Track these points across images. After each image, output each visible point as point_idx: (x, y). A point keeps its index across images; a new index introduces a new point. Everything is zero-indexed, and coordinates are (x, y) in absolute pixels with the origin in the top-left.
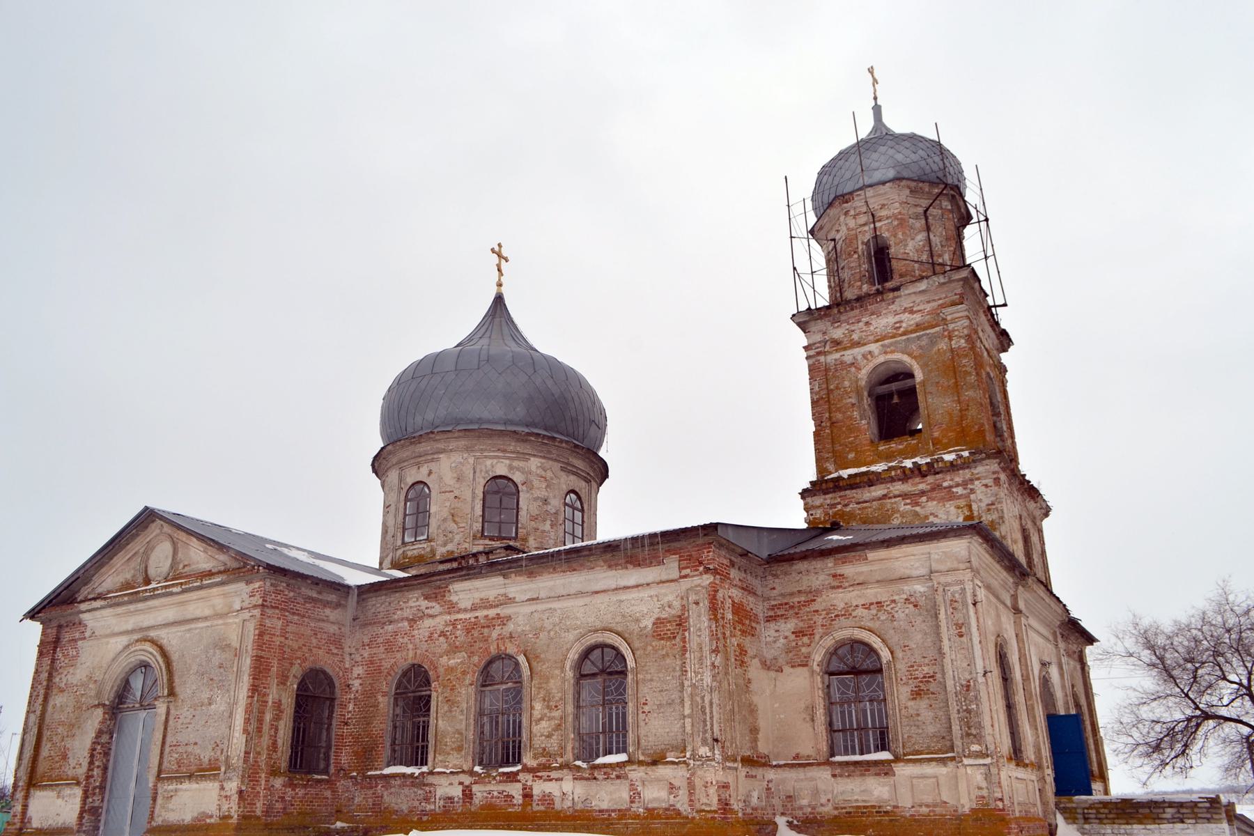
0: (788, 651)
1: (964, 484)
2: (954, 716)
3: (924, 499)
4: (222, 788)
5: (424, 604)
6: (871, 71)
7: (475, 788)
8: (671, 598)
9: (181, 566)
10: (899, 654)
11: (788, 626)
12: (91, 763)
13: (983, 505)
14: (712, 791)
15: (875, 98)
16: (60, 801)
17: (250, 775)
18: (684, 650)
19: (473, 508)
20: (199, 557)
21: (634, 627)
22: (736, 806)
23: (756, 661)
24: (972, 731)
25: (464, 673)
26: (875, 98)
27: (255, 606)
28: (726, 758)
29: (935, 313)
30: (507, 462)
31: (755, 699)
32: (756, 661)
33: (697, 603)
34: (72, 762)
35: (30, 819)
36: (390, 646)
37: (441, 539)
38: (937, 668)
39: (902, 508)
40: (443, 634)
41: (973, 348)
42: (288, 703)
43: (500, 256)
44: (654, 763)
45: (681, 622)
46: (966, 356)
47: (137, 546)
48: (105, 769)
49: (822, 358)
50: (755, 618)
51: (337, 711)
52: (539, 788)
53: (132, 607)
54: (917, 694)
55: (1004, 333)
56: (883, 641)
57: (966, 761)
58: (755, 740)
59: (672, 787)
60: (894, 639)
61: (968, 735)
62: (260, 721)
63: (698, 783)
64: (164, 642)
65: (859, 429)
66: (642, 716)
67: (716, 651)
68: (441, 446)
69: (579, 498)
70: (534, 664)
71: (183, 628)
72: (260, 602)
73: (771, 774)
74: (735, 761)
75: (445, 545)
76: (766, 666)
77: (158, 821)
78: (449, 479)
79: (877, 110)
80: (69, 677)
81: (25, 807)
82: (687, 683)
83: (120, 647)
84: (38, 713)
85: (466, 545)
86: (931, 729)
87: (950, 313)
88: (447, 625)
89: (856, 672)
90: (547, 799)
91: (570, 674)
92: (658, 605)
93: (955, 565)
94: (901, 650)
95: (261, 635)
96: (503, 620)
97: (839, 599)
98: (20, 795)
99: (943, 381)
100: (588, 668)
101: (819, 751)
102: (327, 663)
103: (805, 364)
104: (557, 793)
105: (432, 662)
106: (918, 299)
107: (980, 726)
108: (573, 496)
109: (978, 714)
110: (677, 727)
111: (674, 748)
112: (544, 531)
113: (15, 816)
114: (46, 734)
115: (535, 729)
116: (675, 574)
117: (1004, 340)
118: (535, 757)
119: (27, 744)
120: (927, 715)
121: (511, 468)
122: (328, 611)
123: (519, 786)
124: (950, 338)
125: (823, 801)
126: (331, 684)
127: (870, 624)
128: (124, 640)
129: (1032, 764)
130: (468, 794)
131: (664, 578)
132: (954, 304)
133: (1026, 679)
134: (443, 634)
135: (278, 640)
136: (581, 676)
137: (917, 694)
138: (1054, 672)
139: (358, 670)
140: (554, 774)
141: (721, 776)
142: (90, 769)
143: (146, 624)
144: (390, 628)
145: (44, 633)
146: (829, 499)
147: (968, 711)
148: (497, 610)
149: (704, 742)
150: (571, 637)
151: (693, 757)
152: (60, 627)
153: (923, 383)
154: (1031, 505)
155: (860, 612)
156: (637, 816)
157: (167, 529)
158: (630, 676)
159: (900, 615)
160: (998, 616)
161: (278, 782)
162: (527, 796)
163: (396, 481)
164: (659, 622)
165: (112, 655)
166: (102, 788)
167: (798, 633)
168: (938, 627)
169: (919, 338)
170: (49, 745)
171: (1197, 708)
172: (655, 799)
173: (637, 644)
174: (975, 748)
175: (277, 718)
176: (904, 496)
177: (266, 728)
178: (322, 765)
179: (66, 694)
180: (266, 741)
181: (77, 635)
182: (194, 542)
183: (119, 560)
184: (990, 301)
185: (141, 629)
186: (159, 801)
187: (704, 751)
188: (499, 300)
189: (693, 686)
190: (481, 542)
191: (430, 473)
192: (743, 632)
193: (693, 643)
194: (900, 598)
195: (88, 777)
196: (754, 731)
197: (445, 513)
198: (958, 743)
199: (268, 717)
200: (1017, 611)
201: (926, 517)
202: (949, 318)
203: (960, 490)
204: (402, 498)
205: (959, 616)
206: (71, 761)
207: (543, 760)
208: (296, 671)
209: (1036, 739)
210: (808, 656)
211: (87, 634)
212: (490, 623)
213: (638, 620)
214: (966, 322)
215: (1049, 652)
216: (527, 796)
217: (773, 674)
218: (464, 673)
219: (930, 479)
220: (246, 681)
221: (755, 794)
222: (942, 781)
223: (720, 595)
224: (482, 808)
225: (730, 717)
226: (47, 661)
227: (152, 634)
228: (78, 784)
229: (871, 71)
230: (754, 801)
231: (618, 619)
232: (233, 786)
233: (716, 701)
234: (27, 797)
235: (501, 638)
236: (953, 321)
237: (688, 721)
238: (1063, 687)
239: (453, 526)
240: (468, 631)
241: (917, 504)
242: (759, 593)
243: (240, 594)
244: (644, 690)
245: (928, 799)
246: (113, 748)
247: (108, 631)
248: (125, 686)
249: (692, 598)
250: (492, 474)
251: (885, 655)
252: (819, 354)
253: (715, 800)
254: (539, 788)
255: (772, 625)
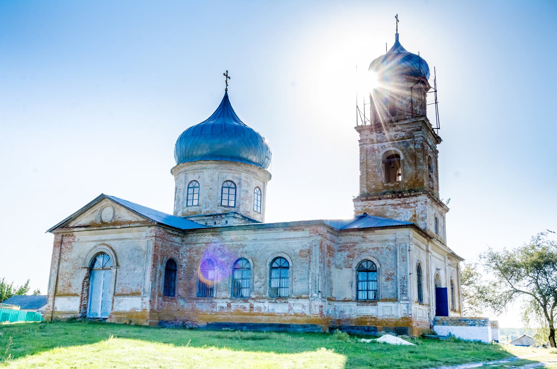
0: (345, 262)
1: (414, 203)
2: (399, 287)
3: (399, 207)
4: (142, 300)
5: (211, 237)
6: (396, 17)
7: (232, 304)
8: (306, 243)
9: (117, 217)
10: (383, 266)
11: (345, 254)
12: (83, 288)
13: (420, 211)
14: (317, 308)
15: (397, 30)
16: (69, 302)
17: (153, 296)
18: (310, 262)
19: (217, 194)
20: (125, 216)
21: (292, 252)
22: (325, 313)
23: (333, 265)
24: (404, 292)
25: (228, 264)
26: (397, 30)
27: (153, 236)
28: (323, 298)
29: (410, 133)
30: (232, 174)
31: (332, 279)
32: (333, 265)
33: (315, 246)
34: (74, 288)
35: (56, 308)
36: (198, 252)
37: (204, 206)
38: (395, 271)
39: (391, 209)
40: (219, 249)
41: (423, 149)
42: (163, 271)
43: (227, 76)
44: (298, 298)
45: (309, 252)
46: (420, 152)
47: (98, 207)
48: (88, 290)
49: (365, 146)
50: (334, 251)
51: (178, 274)
52: (256, 305)
53: (97, 231)
54: (388, 279)
55: (439, 137)
56: (378, 261)
57: (401, 302)
58: (332, 292)
59: (303, 306)
60: (382, 260)
61: (403, 293)
62: (155, 277)
63: (313, 305)
64: (113, 246)
65: (377, 177)
66: (294, 283)
67: (321, 262)
68: (204, 166)
69: (260, 190)
70: (255, 262)
71: (121, 241)
72: (155, 235)
73: (336, 304)
74: (325, 298)
75: (206, 208)
76: (337, 267)
77: (115, 310)
78: (207, 180)
79: (397, 35)
80: (69, 256)
81: (54, 303)
82: (310, 273)
83: (92, 246)
84: (57, 269)
85: (215, 209)
86: (391, 291)
87: (416, 134)
88: (221, 246)
89: (367, 271)
90: (259, 308)
91: (268, 267)
92: (301, 245)
93: (404, 237)
94: (384, 265)
95: (155, 247)
96: (243, 246)
97: (364, 246)
98: (51, 299)
99: (411, 161)
100: (275, 265)
101: (353, 297)
102: (173, 255)
103: (358, 148)
104: (262, 307)
105: (215, 259)
106: (405, 126)
107: (407, 291)
108: (258, 189)
109: (406, 287)
110: (306, 287)
111: (305, 294)
112: (246, 204)
113: (49, 306)
114: (60, 277)
115: (255, 285)
116: (308, 235)
117: (438, 140)
118: (255, 294)
119: (52, 281)
120: (390, 287)
121: (233, 177)
122: (174, 238)
123: (249, 304)
124: (415, 144)
125: (353, 313)
126: (176, 265)
127: (374, 255)
128: (94, 244)
129: (426, 305)
130: (229, 306)
131: (304, 236)
132: (418, 130)
133: (428, 275)
134: (219, 249)
135: (160, 249)
136: (272, 268)
137: (388, 279)
138: (442, 273)
139: (184, 260)
140: (261, 301)
141: (321, 303)
142: (83, 291)
143: (103, 238)
144: (198, 245)
145: (55, 238)
146: (364, 203)
147: (404, 286)
148: (241, 242)
149: (315, 292)
150: (269, 254)
151: (311, 297)
152: (63, 236)
153: (403, 161)
154: (440, 209)
155: (371, 250)
156: (291, 315)
157: (110, 202)
158: (290, 269)
159: (384, 253)
160: (419, 253)
161: (161, 299)
162: (252, 307)
163: (184, 179)
164: (301, 251)
165: (88, 249)
166: (87, 297)
167: (349, 256)
168: (396, 257)
169: (403, 142)
170: (62, 281)
171: (512, 287)
172: (297, 310)
173: (293, 258)
174: (404, 298)
175: (160, 276)
176: (392, 205)
177: (157, 279)
178: (172, 294)
179: (68, 262)
180: (157, 284)
181: (71, 240)
182: (123, 209)
183: (89, 213)
184: (433, 127)
185: (101, 241)
186: (115, 303)
187: (315, 295)
188: (226, 97)
189: (313, 274)
190: (221, 208)
191: (199, 177)
192: (330, 255)
193: (313, 259)
194: (385, 247)
195: (82, 294)
196: (331, 289)
197: (206, 195)
198: (399, 296)
199: (158, 276)
200: (428, 251)
201: (399, 214)
202: (415, 136)
203: (412, 205)
204: (187, 187)
205: (403, 254)
206: (73, 287)
207: (258, 296)
208: (165, 260)
209: (430, 296)
210: (351, 265)
211: (76, 240)
212: (239, 247)
213: (294, 250)
214: (422, 138)
215: (440, 265)
216: (252, 307)
217: (339, 270)
218: (228, 264)
219: (402, 199)
220: (150, 263)
221: (331, 310)
222: (393, 308)
223: (323, 243)
224: (235, 311)
225: (324, 285)
226: (58, 249)
227: (107, 242)
228: (78, 296)
229: (396, 17)
230: (330, 312)
231: (287, 249)
232: (147, 299)
233: (320, 279)
234: (54, 300)
235: (242, 252)
236: (417, 137)
237: (310, 285)
238: (446, 277)
239: (209, 201)
240: (229, 249)
241: (396, 208)
242: (336, 242)
243: (149, 232)
244: (295, 274)
245: (388, 313)
246: (91, 283)
247: (86, 240)
248: (94, 260)
249: (314, 244)
250: (226, 180)
251: (378, 266)
252: (364, 144)
253: (318, 311)
254: (256, 305)
255: (340, 253)
